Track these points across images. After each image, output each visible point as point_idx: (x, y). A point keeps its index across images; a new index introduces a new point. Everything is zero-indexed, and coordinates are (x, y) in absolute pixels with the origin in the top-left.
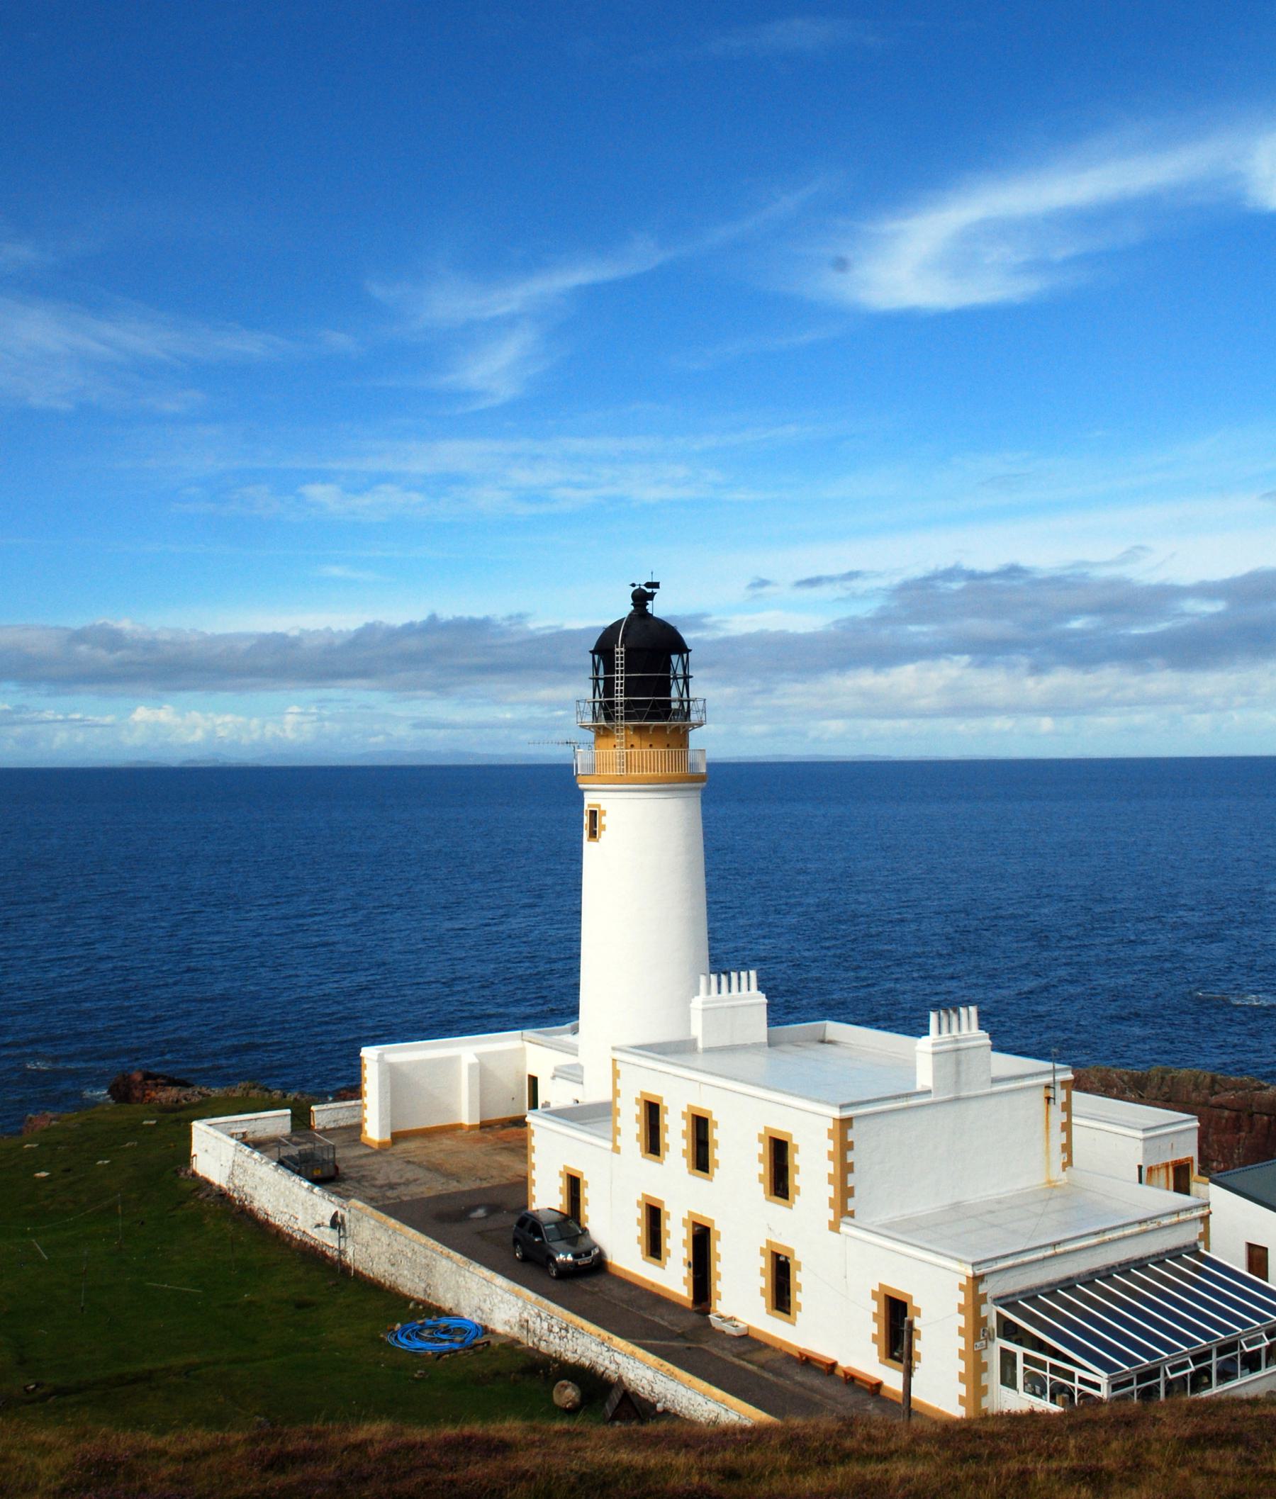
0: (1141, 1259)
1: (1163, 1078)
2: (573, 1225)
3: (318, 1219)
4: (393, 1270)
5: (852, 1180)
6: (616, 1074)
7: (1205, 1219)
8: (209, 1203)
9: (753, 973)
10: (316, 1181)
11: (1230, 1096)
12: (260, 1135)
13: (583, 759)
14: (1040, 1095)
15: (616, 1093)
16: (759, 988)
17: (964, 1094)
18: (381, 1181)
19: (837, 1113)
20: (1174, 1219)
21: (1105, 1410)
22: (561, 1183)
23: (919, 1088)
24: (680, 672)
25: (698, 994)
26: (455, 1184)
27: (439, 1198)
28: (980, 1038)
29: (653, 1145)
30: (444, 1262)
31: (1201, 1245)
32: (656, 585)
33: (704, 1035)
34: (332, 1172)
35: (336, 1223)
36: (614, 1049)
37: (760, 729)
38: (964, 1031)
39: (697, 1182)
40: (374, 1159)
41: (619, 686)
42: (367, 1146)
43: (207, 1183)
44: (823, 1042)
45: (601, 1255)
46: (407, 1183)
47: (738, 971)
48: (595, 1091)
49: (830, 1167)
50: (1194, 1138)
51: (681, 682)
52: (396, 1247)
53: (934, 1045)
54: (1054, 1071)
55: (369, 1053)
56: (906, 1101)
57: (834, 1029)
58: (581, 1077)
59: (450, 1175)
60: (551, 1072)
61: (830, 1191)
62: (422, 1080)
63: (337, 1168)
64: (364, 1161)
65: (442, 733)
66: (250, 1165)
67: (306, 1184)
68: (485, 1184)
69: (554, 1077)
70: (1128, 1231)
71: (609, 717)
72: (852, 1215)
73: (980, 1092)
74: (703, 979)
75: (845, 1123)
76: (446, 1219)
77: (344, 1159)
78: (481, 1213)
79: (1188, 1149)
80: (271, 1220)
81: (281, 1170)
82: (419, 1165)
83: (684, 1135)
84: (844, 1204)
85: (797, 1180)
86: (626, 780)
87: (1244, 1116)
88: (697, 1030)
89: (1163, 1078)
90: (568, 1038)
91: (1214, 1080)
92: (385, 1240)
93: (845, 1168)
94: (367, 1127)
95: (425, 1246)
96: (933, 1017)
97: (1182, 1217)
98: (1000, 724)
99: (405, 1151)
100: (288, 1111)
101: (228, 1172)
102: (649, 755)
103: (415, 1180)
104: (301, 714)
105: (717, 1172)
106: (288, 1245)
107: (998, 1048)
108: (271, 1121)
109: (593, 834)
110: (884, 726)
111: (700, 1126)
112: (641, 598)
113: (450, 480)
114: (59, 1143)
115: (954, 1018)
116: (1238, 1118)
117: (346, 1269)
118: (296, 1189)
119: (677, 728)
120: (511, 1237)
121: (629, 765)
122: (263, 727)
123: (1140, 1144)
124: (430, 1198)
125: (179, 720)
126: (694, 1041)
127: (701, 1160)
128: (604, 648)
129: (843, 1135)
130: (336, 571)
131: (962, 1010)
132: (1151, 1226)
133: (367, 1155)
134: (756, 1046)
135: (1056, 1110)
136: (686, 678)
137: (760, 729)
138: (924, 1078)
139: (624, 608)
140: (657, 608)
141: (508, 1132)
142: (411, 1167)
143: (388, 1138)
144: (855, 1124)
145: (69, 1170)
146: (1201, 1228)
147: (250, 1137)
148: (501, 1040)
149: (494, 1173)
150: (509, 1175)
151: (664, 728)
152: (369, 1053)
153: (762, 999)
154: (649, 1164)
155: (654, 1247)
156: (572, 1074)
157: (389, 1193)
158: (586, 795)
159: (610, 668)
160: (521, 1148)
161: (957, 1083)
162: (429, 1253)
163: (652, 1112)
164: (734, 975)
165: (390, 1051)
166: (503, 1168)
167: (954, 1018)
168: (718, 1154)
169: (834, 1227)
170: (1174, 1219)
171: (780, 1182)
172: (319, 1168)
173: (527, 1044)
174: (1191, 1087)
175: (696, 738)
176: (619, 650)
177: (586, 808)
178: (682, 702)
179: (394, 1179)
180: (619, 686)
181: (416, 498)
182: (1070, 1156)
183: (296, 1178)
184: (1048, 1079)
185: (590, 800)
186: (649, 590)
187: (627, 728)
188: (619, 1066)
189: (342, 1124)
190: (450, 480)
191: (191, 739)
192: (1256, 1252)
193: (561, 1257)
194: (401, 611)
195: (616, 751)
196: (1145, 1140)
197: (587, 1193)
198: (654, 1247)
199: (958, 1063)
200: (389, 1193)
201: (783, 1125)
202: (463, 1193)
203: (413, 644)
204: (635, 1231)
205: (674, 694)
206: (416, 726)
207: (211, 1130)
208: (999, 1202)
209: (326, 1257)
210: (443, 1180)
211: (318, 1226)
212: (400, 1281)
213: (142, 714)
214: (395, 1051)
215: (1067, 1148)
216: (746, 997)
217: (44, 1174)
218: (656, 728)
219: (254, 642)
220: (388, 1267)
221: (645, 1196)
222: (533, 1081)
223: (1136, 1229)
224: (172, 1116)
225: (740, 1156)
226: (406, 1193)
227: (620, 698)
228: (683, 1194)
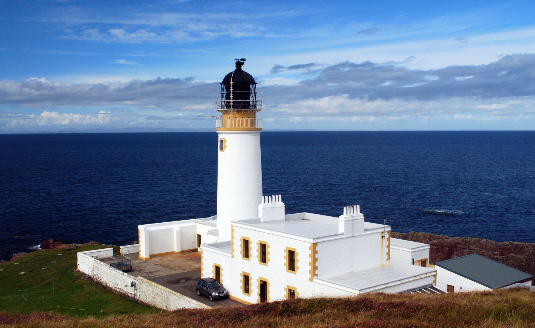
0: (414, 289)
1: (413, 235)
2: (217, 283)
3: (126, 284)
4: (154, 300)
5: (317, 264)
6: (233, 231)
7: (435, 276)
8: (85, 280)
9: (280, 196)
10: (125, 271)
11: (436, 241)
12: (102, 257)
13: (217, 125)
14: (380, 235)
15: (233, 237)
16: (282, 201)
17: (355, 235)
18: (147, 271)
19: (312, 241)
20: (425, 276)
21: (446, 296)
22: (213, 269)
23: (339, 233)
24: (253, 91)
25: (261, 203)
26: (173, 271)
27: (169, 276)
29: (246, 254)
30: (173, 296)
31: (434, 285)
32: (244, 60)
33: (263, 217)
34: (130, 269)
35: (133, 285)
36: (232, 222)
37: (271, 120)
38: (355, 213)
39: (262, 266)
40: (144, 264)
42: (141, 260)
43: (84, 274)
44: (303, 220)
45: (228, 292)
46: (157, 271)
47: (275, 195)
48: (224, 237)
49: (310, 260)
50: (428, 252)
51: (253, 95)
52: (155, 292)
53: (345, 218)
54: (385, 227)
55: (141, 227)
56: (335, 237)
57: (307, 215)
58: (218, 234)
59: (171, 269)
60: (207, 232)
61: (309, 268)
62: (160, 237)
63: (131, 267)
64: (140, 264)
65: (157, 121)
67: (121, 272)
68: (184, 271)
69: (208, 234)
70: (410, 280)
71: (228, 107)
72: (317, 275)
73: (360, 234)
74: (263, 197)
75: (315, 244)
76: (174, 282)
77: (133, 264)
78: (184, 281)
79: (426, 255)
80: (108, 285)
81: (112, 268)
82: (160, 265)
83: (257, 251)
84: (314, 272)
85: (297, 264)
86: (234, 129)
87: (440, 248)
89: (413, 235)
90: (211, 221)
91: (430, 236)
92: (151, 290)
93: (315, 260)
94: (141, 253)
95: (166, 291)
96: (345, 208)
97: (428, 275)
98: (355, 119)
99: (155, 261)
100: (112, 248)
101: (91, 270)
102: (241, 120)
104: (105, 114)
105: (269, 263)
106: (115, 294)
107: (365, 221)
109: (222, 149)
110: (315, 119)
111: (263, 248)
112: (239, 64)
113: (163, 29)
114: (27, 262)
115: (352, 209)
116: (438, 248)
117: (137, 301)
118: (117, 274)
119: (252, 111)
120: (195, 288)
121: (235, 124)
122: (91, 118)
123: (410, 254)
124: (165, 276)
125: (59, 116)
126: (260, 219)
127: (264, 259)
128: (226, 81)
129: (314, 249)
130: (121, 61)
131: (355, 206)
132: (417, 278)
133: (141, 263)
134: (281, 221)
135: (385, 240)
136: (255, 93)
137: (271, 120)
138: (341, 229)
139: (233, 68)
140: (244, 68)
141: (193, 254)
142: (157, 266)
143: (148, 257)
144: (318, 245)
145: (32, 271)
146: (434, 279)
147: (99, 257)
149: (187, 267)
150: (193, 268)
151: (247, 111)
152: (141, 227)
153: (283, 205)
154: (245, 261)
155: (247, 290)
156: (215, 233)
157: (150, 275)
158: (219, 135)
159: (228, 89)
160: (198, 259)
161: (352, 231)
162: (167, 293)
163: (246, 243)
164: (273, 196)
165: (148, 227)
166: (190, 266)
167: (352, 209)
168: (269, 257)
169: (311, 280)
170: (425, 276)
171: (292, 265)
172: (126, 267)
173: (197, 224)
174: (422, 238)
176: (232, 83)
177: (219, 139)
178: (253, 102)
179: (152, 270)
181: (153, 35)
182: (389, 256)
183: (118, 270)
184: (383, 230)
185: (220, 137)
186: (242, 62)
187: (234, 111)
188: (234, 228)
189: (131, 252)
190: (163, 29)
191: (63, 123)
192: (451, 288)
193: (214, 294)
194: (146, 76)
195: (231, 119)
196: (412, 252)
197: (222, 272)
198: (247, 290)
199: (353, 224)
200: (150, 275)
201: (292, 246)
202: (177, 274)
203: (150, 88)
204: (240, 284)
205: (251, 99)
206: (148, 118)
207: (85, 255)
208: (366, 271)
209: (129, 297)
210: (169, 270)
211: (127, 286)
212: (156, 304)
213: (45, 114)
214: (150, 226)
215: (388, 253)
216: (277, 204)
217: (23, 273)
218: (245, 111)
219: (92, 87)
220: (152, 299)
221: (243, 272)
222: (199, 236)
223: (413, 279)
224: (68, 252)
226: (157, 275)
227: (231, 100)
228: (257, 271)
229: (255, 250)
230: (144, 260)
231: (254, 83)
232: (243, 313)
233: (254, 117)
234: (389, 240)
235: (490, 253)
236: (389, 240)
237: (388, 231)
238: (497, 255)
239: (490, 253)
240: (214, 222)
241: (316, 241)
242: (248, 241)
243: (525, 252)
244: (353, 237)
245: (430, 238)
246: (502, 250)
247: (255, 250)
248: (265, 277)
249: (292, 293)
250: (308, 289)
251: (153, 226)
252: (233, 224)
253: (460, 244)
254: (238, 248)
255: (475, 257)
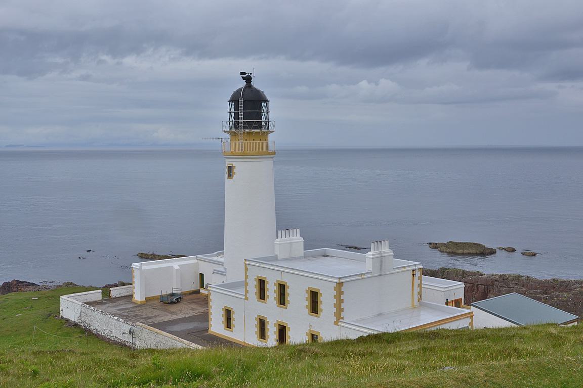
6: (246, 269)
7: (471, 317)
9: (298, 230)
14: (411, 273)
15: (246, 277)
26: (176, 316)
28: (391, 252)
29: (262, 295)
41: (241, 115)
42: (135, 303)
44: (324, 256)
46: (155, 317)
51: (265, 113)
60: (213, 271)
66: (89, 312)
68: (187, 316)
69: (214, 273)
71: (236, 128)
75: (340, 284)
79: (461, 295)
88: (277, 252)
92: (153, 337)
94: (134, 296)
100: (101, 291)
103: (158, 315)
105: (289, 306)
108: (93, 295)
111: (282, 288)
116: (473, 286)
118: (111, 320)
126: (277, 256)
127: (282, 299)
131: (132, 266)
136: (267, 113)
141: (198, 297)
148: (168, 262)
155: (263, 334)
163: (262, 283)
164: (291, 231)
168: (289, 298)
169: (336, 323)
171: (314, 307)
175: (271, 137)
180: (241, 115)
188: (248, 266)
198: (263, 334)
204: (255, 329)
205: (263, 119)
207: (70, 299)
211: (124, 333)
222: (202, 275)
225: (298, 298)
227: (241, 120)
228: (273, 314)
229: (272, 292)
230: (139, 303)
231: (266, 101)
232: (247, 364)
233: (267, 140)
234: (420, 278)
235: (532, 291)
236: (420, 278)
237: (419, 269)
238: (540, 293)
239: (532, 291)
240: (220, 259)
241: (341, 281)
242: (264, 281)
243: (571, 290)
244: (380, 275)
245: (463, 275)
246: (545, 288)
247: (272, 292)
248: (284, 321)
249: (314, 337)
250: (329, 333)
251: (156, 263)
252: (247, 262)
253: (497, 281)
254: (253, 289)
255: (514, 295)
